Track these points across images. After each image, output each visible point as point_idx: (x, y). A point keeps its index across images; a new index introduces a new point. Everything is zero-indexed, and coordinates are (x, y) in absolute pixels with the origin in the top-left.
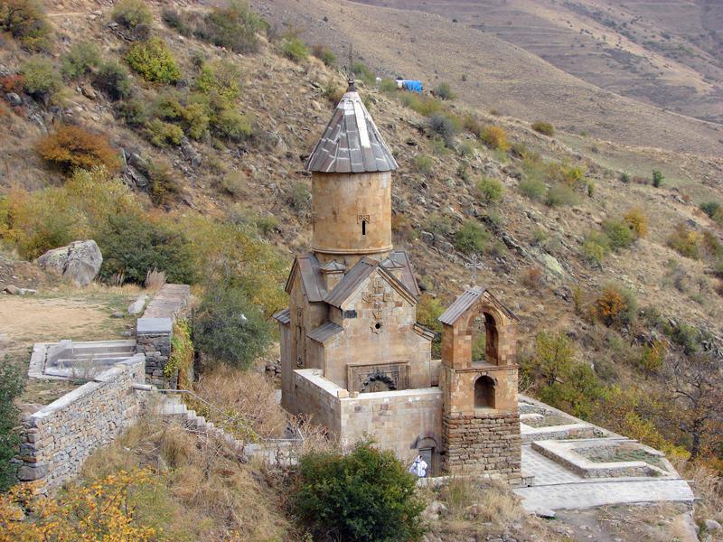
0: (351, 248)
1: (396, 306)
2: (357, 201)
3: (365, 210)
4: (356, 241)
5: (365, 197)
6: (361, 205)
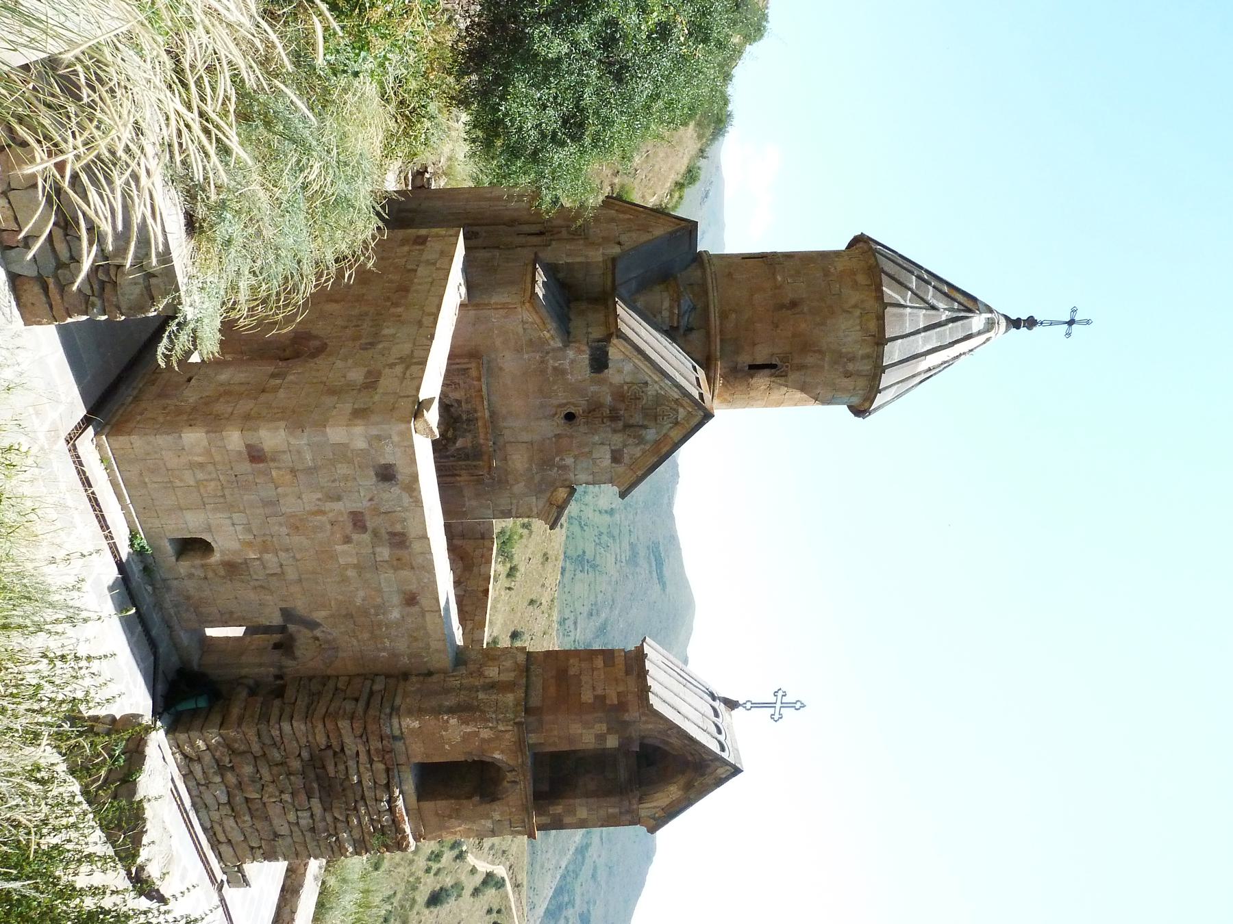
0: (722, 340)
1: (613, 451)
2: (820, 352)
3: (801, 367)
4: (737, 352)
5: (826, 367)
6: (810, 359)
